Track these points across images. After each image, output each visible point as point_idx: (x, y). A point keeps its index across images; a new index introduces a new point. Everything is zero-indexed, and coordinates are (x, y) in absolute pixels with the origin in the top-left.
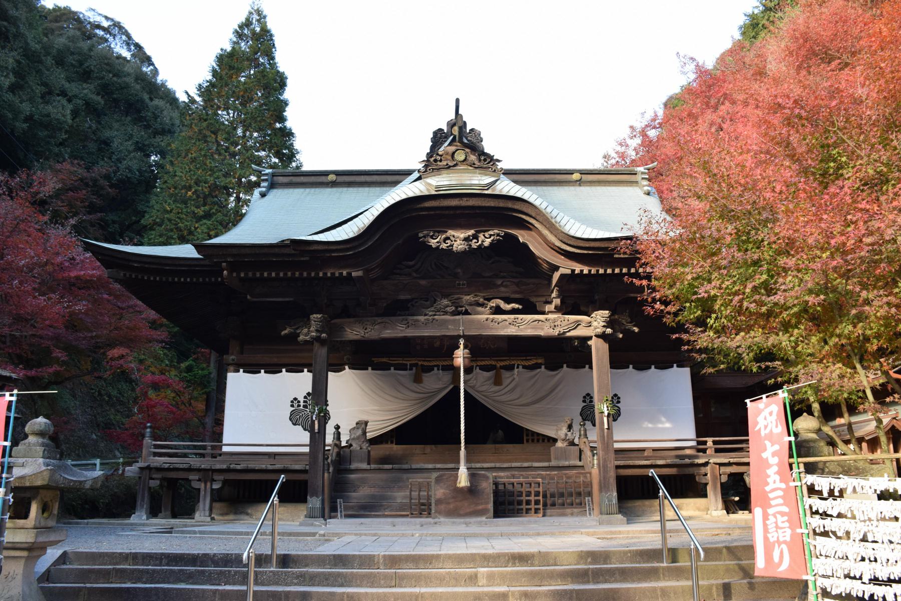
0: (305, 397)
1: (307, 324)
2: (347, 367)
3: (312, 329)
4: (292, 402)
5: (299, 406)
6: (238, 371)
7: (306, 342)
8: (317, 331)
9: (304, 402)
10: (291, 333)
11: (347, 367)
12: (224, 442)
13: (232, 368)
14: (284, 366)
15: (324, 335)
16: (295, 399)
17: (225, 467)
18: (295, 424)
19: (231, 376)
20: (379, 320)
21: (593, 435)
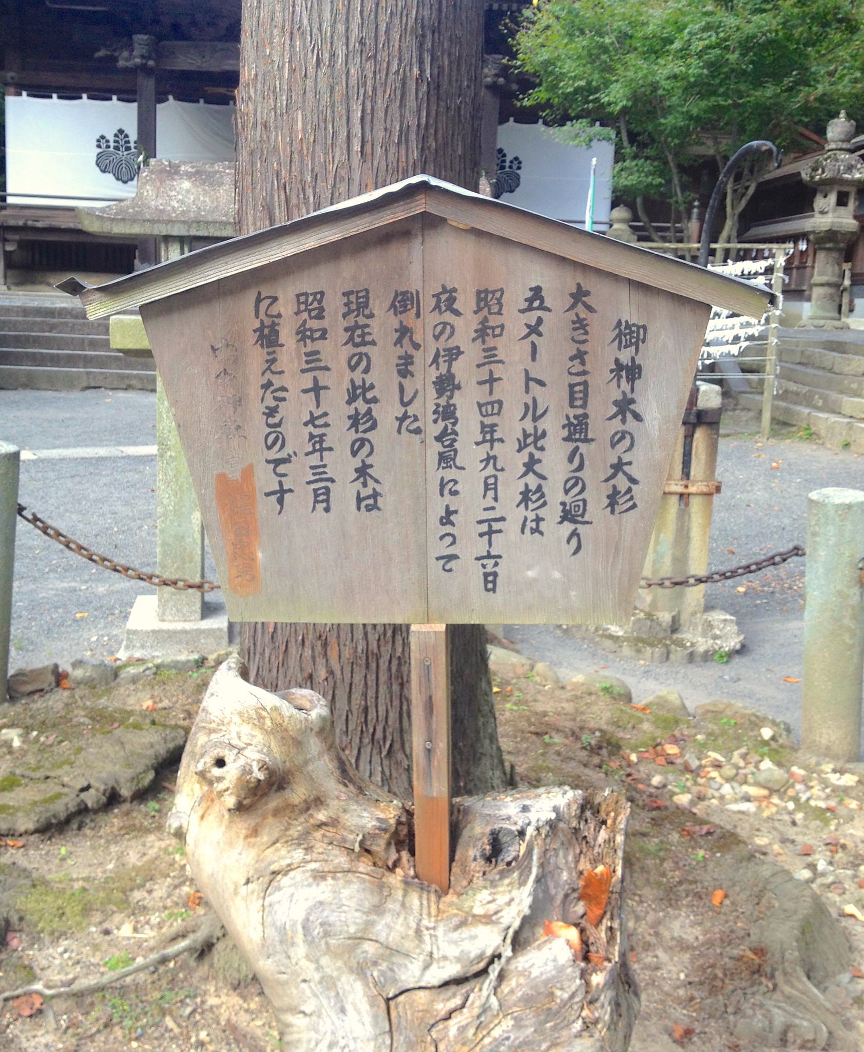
0: (116, 135)
1: (130, 47)
2: (171, 97)
3: (135, 53)
4: (98, 141)
5: (108, 147)
6: (20, 95)
7: (126, 70)
8: (143, 57)
9: (115, 142)
10: (107, 56)
11: (171, 97)
12: (10, 189)
13: (12, 90)
14: (85, 90)
15: (151, 63)
16: (103, 137)
17: (21, 223)
18: (104, 171)
19: (11, 102)
20: (220, 45)
21: (92, 891)
